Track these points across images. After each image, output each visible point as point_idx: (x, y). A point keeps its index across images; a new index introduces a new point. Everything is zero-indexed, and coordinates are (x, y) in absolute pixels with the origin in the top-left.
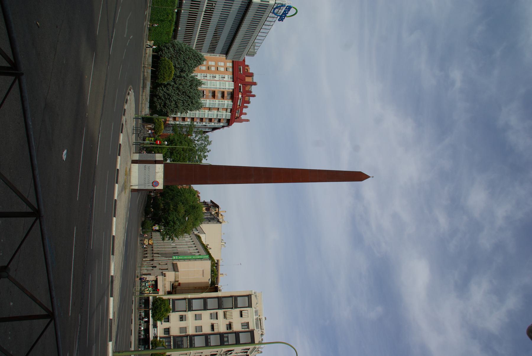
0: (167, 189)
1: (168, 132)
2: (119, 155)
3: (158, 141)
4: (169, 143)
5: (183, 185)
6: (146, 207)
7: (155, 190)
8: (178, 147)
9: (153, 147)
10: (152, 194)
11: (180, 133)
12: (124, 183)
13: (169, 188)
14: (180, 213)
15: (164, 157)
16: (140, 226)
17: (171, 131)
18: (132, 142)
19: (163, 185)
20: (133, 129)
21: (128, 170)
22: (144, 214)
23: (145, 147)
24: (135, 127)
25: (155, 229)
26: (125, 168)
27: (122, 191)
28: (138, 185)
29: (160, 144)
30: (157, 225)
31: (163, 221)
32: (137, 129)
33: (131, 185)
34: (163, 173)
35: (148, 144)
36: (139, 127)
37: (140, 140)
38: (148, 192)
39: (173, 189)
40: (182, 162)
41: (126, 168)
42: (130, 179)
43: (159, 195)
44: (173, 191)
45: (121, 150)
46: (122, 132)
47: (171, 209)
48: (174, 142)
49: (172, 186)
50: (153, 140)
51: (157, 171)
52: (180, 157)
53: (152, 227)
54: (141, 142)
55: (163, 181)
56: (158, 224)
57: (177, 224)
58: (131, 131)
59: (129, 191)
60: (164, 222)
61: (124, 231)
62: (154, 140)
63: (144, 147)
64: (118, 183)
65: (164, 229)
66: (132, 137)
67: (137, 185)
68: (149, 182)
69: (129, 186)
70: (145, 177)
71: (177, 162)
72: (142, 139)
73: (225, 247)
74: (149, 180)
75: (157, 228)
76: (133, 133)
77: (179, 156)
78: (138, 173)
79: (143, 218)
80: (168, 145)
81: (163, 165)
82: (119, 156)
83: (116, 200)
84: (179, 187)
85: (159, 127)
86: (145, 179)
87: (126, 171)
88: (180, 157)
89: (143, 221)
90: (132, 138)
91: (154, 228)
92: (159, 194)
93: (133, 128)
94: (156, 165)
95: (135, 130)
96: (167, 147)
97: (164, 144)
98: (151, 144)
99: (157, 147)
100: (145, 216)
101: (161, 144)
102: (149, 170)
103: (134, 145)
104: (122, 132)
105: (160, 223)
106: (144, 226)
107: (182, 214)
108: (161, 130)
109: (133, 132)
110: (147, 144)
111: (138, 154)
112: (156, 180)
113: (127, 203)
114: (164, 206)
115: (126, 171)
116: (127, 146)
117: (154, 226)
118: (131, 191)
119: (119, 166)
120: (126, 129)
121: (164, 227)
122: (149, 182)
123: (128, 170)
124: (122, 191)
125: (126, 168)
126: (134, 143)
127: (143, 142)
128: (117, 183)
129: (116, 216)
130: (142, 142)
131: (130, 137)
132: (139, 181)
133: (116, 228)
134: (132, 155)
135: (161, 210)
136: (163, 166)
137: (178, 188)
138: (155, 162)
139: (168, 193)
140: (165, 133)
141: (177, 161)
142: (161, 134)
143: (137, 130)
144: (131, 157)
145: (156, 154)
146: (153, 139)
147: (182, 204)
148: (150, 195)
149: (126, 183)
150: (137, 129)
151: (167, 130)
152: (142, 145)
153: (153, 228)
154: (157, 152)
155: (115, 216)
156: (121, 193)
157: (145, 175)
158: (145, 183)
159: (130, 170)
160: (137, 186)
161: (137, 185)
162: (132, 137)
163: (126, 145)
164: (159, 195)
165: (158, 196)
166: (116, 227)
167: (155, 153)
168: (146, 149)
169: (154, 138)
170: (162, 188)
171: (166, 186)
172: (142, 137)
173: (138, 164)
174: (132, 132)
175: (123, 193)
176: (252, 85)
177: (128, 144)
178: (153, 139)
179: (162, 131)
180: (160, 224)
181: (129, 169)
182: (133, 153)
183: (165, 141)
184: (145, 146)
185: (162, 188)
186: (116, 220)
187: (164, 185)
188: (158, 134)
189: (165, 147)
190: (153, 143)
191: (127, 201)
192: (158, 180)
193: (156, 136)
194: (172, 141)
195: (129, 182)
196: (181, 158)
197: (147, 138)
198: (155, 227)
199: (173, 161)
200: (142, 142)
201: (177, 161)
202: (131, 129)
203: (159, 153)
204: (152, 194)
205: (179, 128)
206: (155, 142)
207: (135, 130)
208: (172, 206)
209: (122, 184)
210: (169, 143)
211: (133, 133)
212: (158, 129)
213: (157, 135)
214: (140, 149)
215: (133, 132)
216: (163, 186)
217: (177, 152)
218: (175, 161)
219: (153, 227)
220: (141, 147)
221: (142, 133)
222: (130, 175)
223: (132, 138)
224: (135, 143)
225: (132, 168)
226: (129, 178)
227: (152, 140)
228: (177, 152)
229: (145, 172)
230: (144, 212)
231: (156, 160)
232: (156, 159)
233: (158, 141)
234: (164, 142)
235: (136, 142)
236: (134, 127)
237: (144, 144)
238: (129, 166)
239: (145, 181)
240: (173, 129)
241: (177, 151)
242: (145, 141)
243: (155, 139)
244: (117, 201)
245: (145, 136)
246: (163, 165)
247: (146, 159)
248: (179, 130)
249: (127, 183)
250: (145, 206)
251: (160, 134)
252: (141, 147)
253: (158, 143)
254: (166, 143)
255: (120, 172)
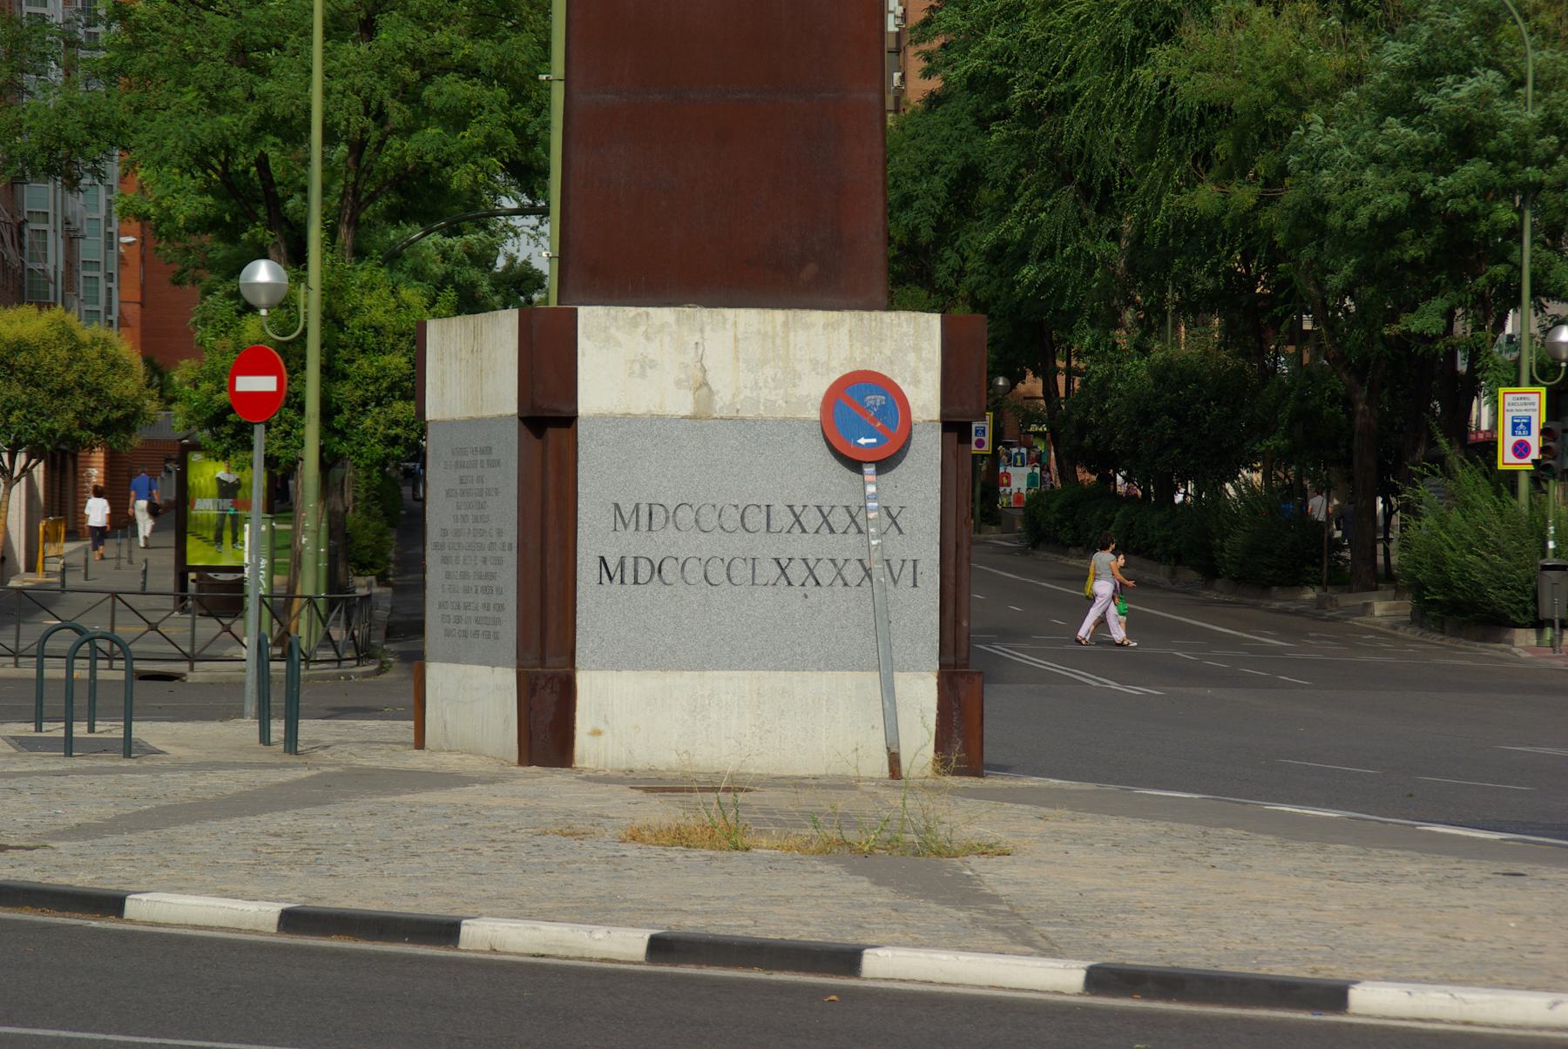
0: (941, 272)
1: (90, 248)
2: (447, 931)
3: (245, 384)
4: (260, 232)
5: (892, 26)
6: (1210, 572)
7: (954, 427)
8: (327, 93)
9: (329, 461)
10: (1018, 480)
11: (112, 73)
12: (855, 871)
13: (926, 235)
14: (1298, 69)
15: (470, 303)
16: (1493, 649)
17: (76, 203)
18: (265, 755)
19: (889, 317)
20: (69, 745)
21: (660, 812)
22: (1310, 594)
23: (335, 585)
24: (27, 729)
25: (1534, 441)
26: (632, 850)
27: (966, 894)
28: (886, 670)
29: (288, 357)
30: (1481, 414)
31: (1424, 320)
32: (55, 701)
33: (878, 765)
34: (704, 314)
35: (282, 550)
36: (31, 672)
37: (233, 651)
38: (993, 535)
39: (938, 183)
40: (546, 46)
41: (635, 837)
42: (798, 783)
43: (1032, 385)
44: (969, 178)
45: (376, 906)
46: (112, 904)
47: (1244, 195)
48: (240, 163)
49: (906, 202)
50: (220, 471)
51: (681, 404)
52: (469, 70)
53: (1514, 475)
54: (250, 640)
55: (818, 317)
56: (1463, 391)
57: (1482, 98)
58: (100, 782)
59: (954, 792)
60: (1439, 303)
61: (1544, 871)
62: (225, 456)
63: (331, 604)
64: (850, 938)
65: (1540, 308)
66: (180, 766)
67: (888, 691)
68: (840, 519)
69: (894, 798)
70: (770, 571)
71: (541, 109)
72: (208, 627)
73: (497, 492)
74: (812, 519)
75: (1522, 412)
76: (128, 747)
77: (450, 89)
78: (718, 681)
79: (1366, 609)
80: (296, 257)
81: (583, 311)
82: (464, 929)
83: (1099, 979)
84: (919, 87)
85: (32, 380)
86: (797, 572)
87: (680, 838)
88: (469, 70)
89: (1406, 606)
90: (198, 767)
91: (1521, 449)
92: (1015, 378)
93: (48, 744)
94: (602, 419)
95: (80, 729)
96: (329, 269)
97: (286, 305)
98: (280, 498)
99: (328, 411)
100: (1339, 580)
101: (283, 348)
102: (671, 518)
103: (308, 729)
104: (112, 904)
105: (1451, 356)
106: (1494, 595)
107: (1326, 39)
108: (78, 347)
109: (102, 747)
110: (284, 559)
111: (437, 674)
112: (815, 414)
113: (1141, 828)
114: (1194, 307)
115: (680, 838)
116: (319, 822)
117: (1489, 447)
118: (973, 765)
119: (600, 933)
120: (62, 845)
121: (1516, 303)
122: (840, 519)
123: (660, 812)
124: (966, 894)
125: (635, 837)
126: (265, 737)
127: (251, 603)
128: (847, 960)
129: (1333, 971)
130: (252, 624)
131: (182, 786)
132: (830, 663)
133: (1510, 986)
134: (451, 762)
135: (1262, 352)
136: (599, 310)
137: (934, 101)
138: (551, 433)
139: (1003, 257)
140: (126, 294)
141: (521, 114)
142: (126, 349)
143: (81, 700)
144: (472, 764)
145: (431, 414)
146: (207, 473)
147: (1167, 35)
148: (1034, 505)
149: (851, 835)
150: (55, 701)
151: (70, 264)
152: (303, 628)
153: (1525, 465)
154: (400, 409)
155: (1334, 996)
156: (995, 899)
157: (741, 571)
158: (853, 572)
159: (657, 785)
160: (902, 681)
161: (888, 691)
162: (180, 766)
163: (297, 836)
164: (1032, 385)
165: (1050, 390)
166: (1492, 983)
167: (419, 424)
168: (363, 567)
169: (195, 457)
170: (934, 321)
171: (898, 280)
172: (177, 625)
173: (587, 683)
174: (104, 761)
175: (992, 874)
176: (693, 418)
177: (285, 820)
178: (207, 473)
179: (85, 335)
180: (1462, 367)
181: (655, 800)
182: (420, 743)
183: (236, 295)
184: (310, 582)
185: (934, 321)
186: (1395, 974)
187: (882, 298)
188: (129, 386)
189: (333, 291)
190: (270, 462)
191: (1115, 825)
192: (815, 388)
193: (176, 422)
194: (229, 186)
195: (844, 802)
196: (485, 51)
197: (199, 554)
198: (1507, 442)
199: (528, 175)
200: (252, 624)
201: (521, 114)
202: (68, 783)
203: (411, 387)
204: (1018, 480)
205: (29, 80)
206: (259, 436)
207: (80, 729)
208: (1205, 197)
209: (864, 884)
210: (260, 232)
211: (128, 747)
212: (63, 392)
213: (151, 406)
214: (364, 652)
215: (102, 747)
216: (904, 316)
217: (397, 113)
218: (532, 141)
219: (1507, 459)
220: (338, 634)
221: (128, 628)
222: (737, 785)
223: (198, 767)
224: (278, 728)
225: (639, 764)
226: (770, 797)
227: (227, 490)
228: (397, 113)
229: (694, 572)
230: (1279, 600)
231: (510, 407)
232: (501, 420)
233: (245, 384)
234: (251, 309)
235: (251, 706)
236: (23, 744)
237: (290, 596)
238: (602, 791)
239: (825, 572)
240: (50, 171)
241: (380, 116)
242: (239, 585)
243: (204, 436)
244: (1112, 958)
245: (169, 582)
246: (583, 311)
247: (511, 558)
248: (55, 74)
249: (846, 820)
250: (1193, 575)
251: (140, 368)
252: (338, 634)
253: (267, 384)
254: (263, 272)
255: (691, 924)
